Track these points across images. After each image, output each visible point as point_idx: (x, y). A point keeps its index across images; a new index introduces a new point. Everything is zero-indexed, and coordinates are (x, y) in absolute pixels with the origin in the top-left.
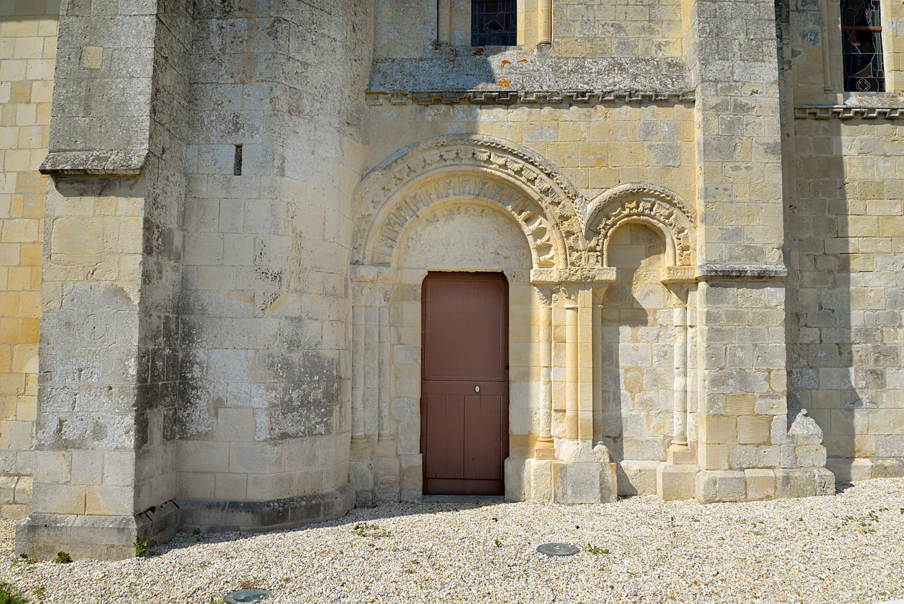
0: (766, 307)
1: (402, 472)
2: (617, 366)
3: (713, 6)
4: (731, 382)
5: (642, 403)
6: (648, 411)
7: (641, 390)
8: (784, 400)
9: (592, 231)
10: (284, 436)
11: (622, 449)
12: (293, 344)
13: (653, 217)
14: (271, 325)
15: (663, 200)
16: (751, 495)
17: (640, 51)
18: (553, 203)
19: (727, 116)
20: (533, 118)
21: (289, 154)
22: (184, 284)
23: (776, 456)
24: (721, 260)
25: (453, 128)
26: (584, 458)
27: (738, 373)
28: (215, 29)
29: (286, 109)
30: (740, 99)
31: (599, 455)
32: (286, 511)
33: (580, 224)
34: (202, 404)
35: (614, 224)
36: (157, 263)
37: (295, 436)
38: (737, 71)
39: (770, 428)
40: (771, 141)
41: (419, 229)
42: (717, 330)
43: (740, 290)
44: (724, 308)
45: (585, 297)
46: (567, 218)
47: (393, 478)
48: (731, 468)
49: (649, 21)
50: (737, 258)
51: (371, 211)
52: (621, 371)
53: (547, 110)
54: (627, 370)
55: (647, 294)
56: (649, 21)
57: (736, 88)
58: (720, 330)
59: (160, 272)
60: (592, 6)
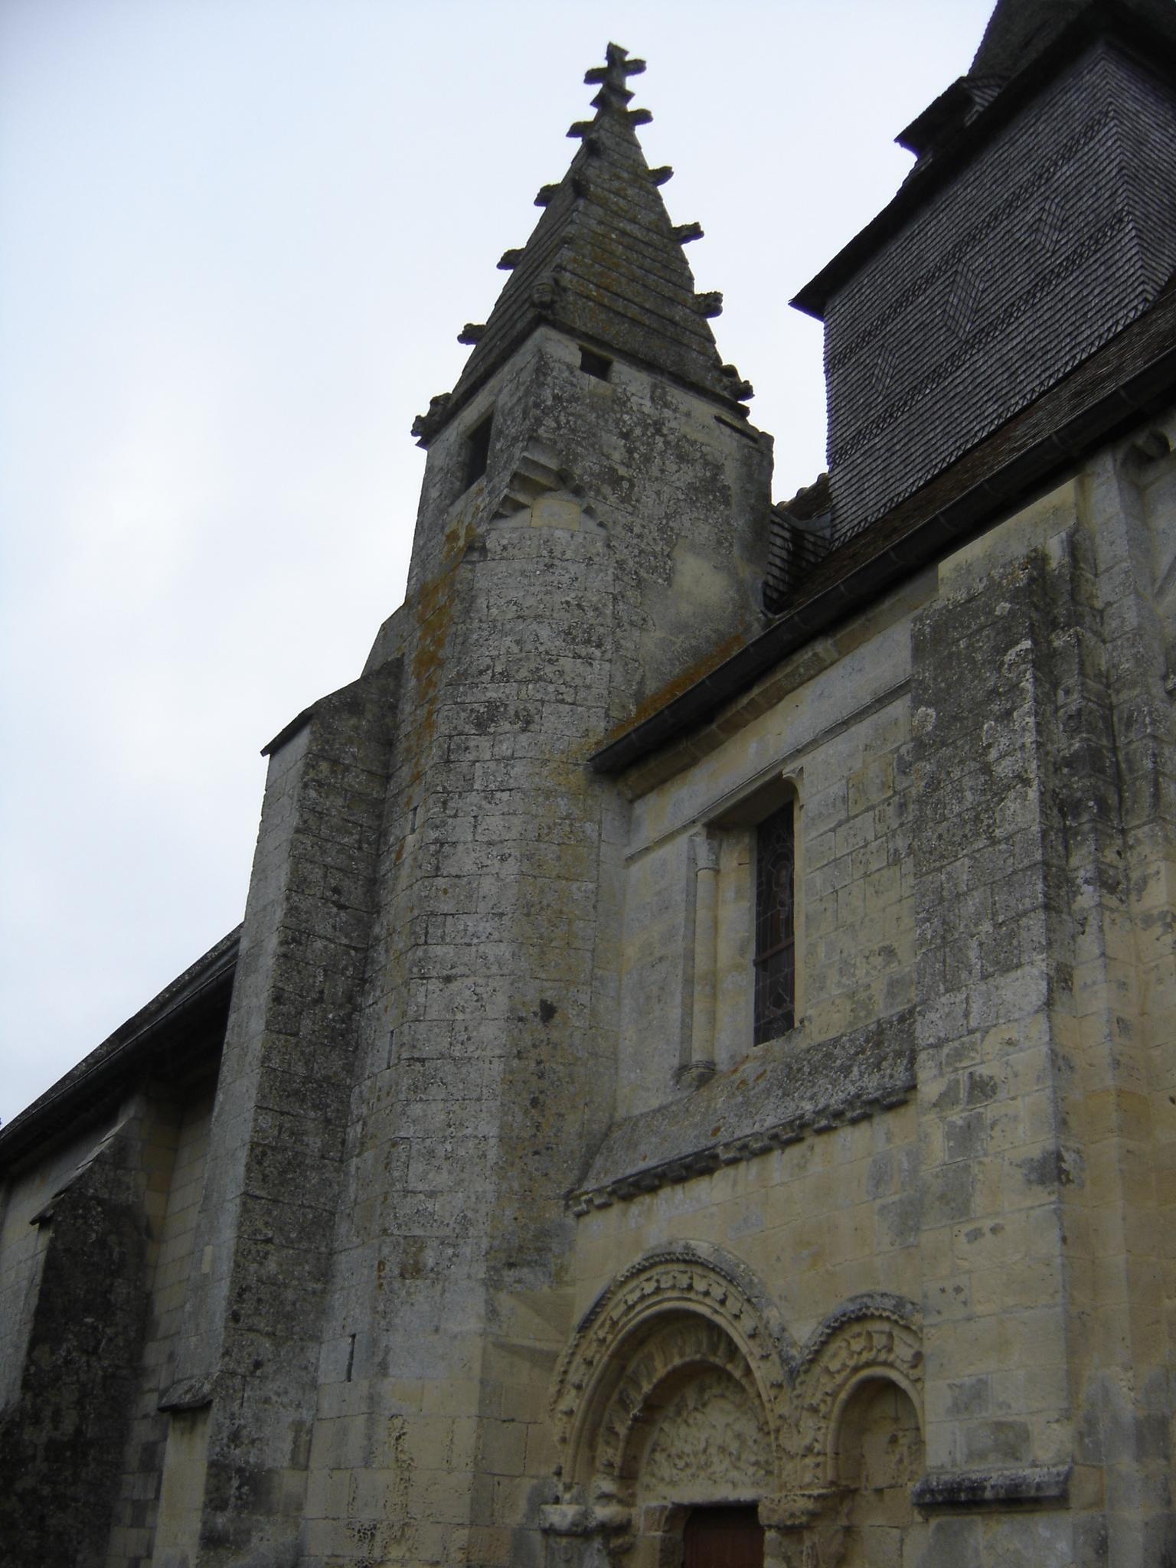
13: (891, 1365)
29: (397, 1272)
38: (976, 1007)
50: (982, 1456)
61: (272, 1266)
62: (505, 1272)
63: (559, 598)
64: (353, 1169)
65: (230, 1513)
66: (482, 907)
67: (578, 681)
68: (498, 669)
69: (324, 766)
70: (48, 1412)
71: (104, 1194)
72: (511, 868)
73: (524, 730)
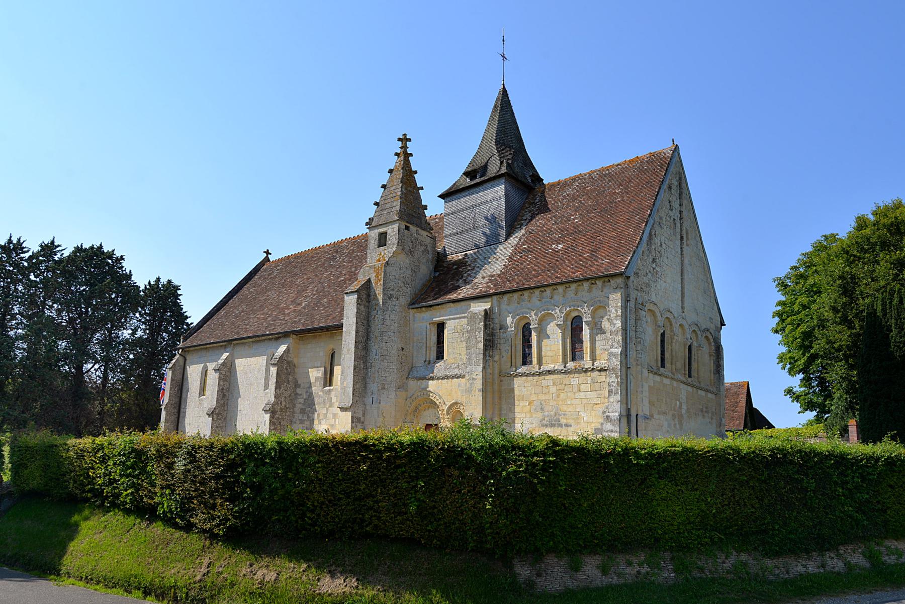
25: (423, 386)
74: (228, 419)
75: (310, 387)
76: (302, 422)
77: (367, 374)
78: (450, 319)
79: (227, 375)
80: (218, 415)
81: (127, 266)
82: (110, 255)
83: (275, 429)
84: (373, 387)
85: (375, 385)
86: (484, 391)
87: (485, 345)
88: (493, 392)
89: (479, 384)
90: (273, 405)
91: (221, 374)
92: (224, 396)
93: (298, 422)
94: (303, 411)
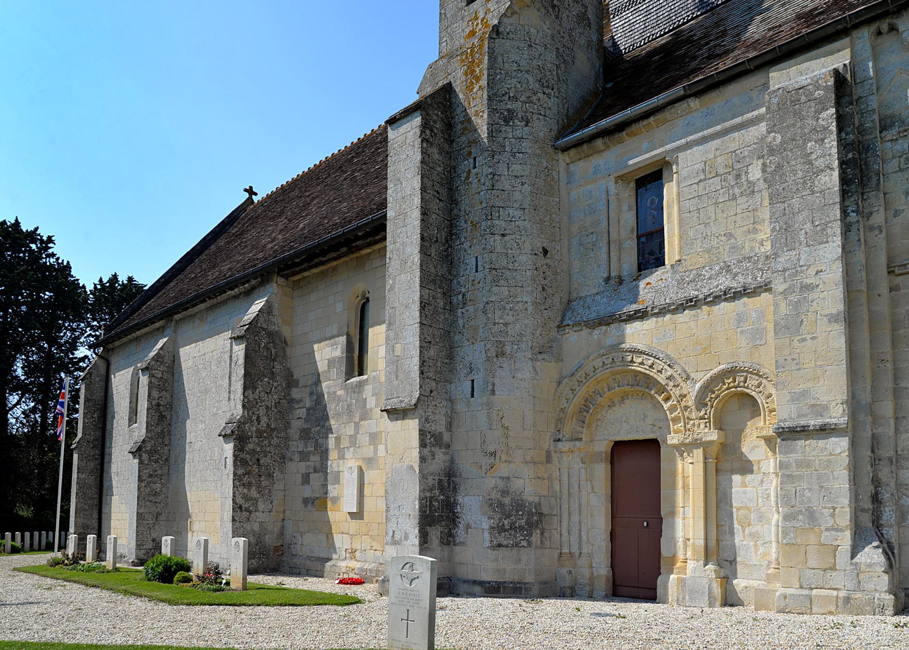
0: (831, 454)
1: (592, 578)
2: (731, 506)
3: (782, 206)
4: (801, 517)
5: (751, 535)
6: (756, 542)
7: (749, 525)
8: (848, 535)
9: (701, 403)
10: (500, 545)
11: (736, 570)
12: (505, 492)
14: (490, 482)
15: (751, 373)
16: (815, 610)
17: (746, 251)
18: (674, 386)
19: (793, 298)
20: (659, 324)
21: (497, 381)
22: (452, 461)
23: (841, 580)
24: (791, 418)
25: (609, 341)
26: (697, 574)
27: (806, 510)
28: (460, 314)
29: (494, 354)
30: (805, 281)
31: (708, 572)
32: (499, 588)
33: (690, 401)
34: (461, 526)
35: (718, 396)
36: (431, 451)
37: (507, 546)
39: (835, 556)
40: (834, 311)
41: (604, 412)
42: (788, 476)
43: (808, 442)
44: (793, 457)
45: (698, 453)
46: (685, 396)
47: (585, 581)
48: (801, 587)
49: (753, 224)
50: (804, 416)
51: (566, 405)
52: (734, 510)
53: (668, 316)
54: (738, 509)
55: (753, 449)
56: (753, 224)
57: (802, 272)
58: (791, 475)
59: (433, 456)
60: (709, 223)
61: (432, 353)
62: (539, 356)
63: (535, 63)
64: (460, 314)
65: (428, 449)
66: (516, 205)
67: (545, 105)
68: (512, 95)
69: (428, 132)
70: (254, 418)
71: (265, 326)
72: (527, 188)
73: (526, 125)
74: (172, 460)
75: (318, 382)
76: (304, 456)
77: (453, 323)
78: (680, 149)
79: (166, 383)
80: (151, 453)
81: (62, 251)
82: (32, 235)
83: (248, 473)
84: (472, 353)
85: (479, 346)
86: (850, 319)
87: (844, 181)
88: (873, 323)
89: (830, 297)
90: (241, 423)
91: (152, 376)
92: (162, 417)
93: (296, 457)
94: (305, 435)
